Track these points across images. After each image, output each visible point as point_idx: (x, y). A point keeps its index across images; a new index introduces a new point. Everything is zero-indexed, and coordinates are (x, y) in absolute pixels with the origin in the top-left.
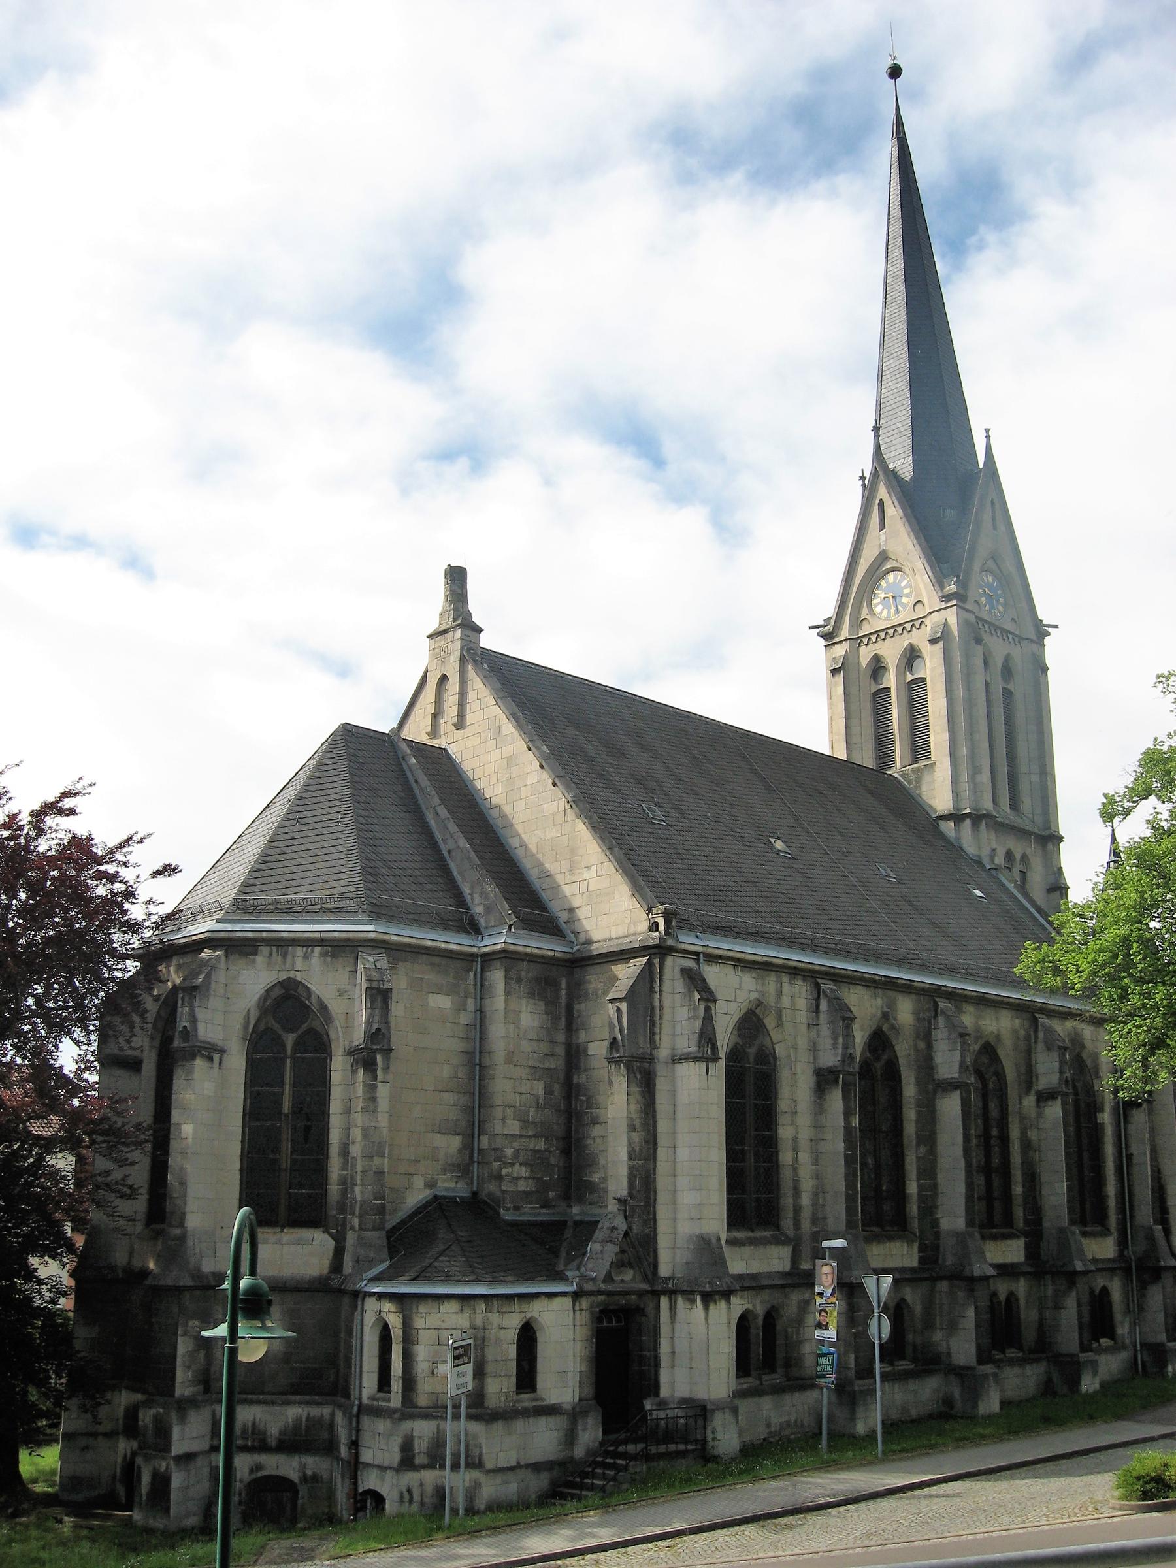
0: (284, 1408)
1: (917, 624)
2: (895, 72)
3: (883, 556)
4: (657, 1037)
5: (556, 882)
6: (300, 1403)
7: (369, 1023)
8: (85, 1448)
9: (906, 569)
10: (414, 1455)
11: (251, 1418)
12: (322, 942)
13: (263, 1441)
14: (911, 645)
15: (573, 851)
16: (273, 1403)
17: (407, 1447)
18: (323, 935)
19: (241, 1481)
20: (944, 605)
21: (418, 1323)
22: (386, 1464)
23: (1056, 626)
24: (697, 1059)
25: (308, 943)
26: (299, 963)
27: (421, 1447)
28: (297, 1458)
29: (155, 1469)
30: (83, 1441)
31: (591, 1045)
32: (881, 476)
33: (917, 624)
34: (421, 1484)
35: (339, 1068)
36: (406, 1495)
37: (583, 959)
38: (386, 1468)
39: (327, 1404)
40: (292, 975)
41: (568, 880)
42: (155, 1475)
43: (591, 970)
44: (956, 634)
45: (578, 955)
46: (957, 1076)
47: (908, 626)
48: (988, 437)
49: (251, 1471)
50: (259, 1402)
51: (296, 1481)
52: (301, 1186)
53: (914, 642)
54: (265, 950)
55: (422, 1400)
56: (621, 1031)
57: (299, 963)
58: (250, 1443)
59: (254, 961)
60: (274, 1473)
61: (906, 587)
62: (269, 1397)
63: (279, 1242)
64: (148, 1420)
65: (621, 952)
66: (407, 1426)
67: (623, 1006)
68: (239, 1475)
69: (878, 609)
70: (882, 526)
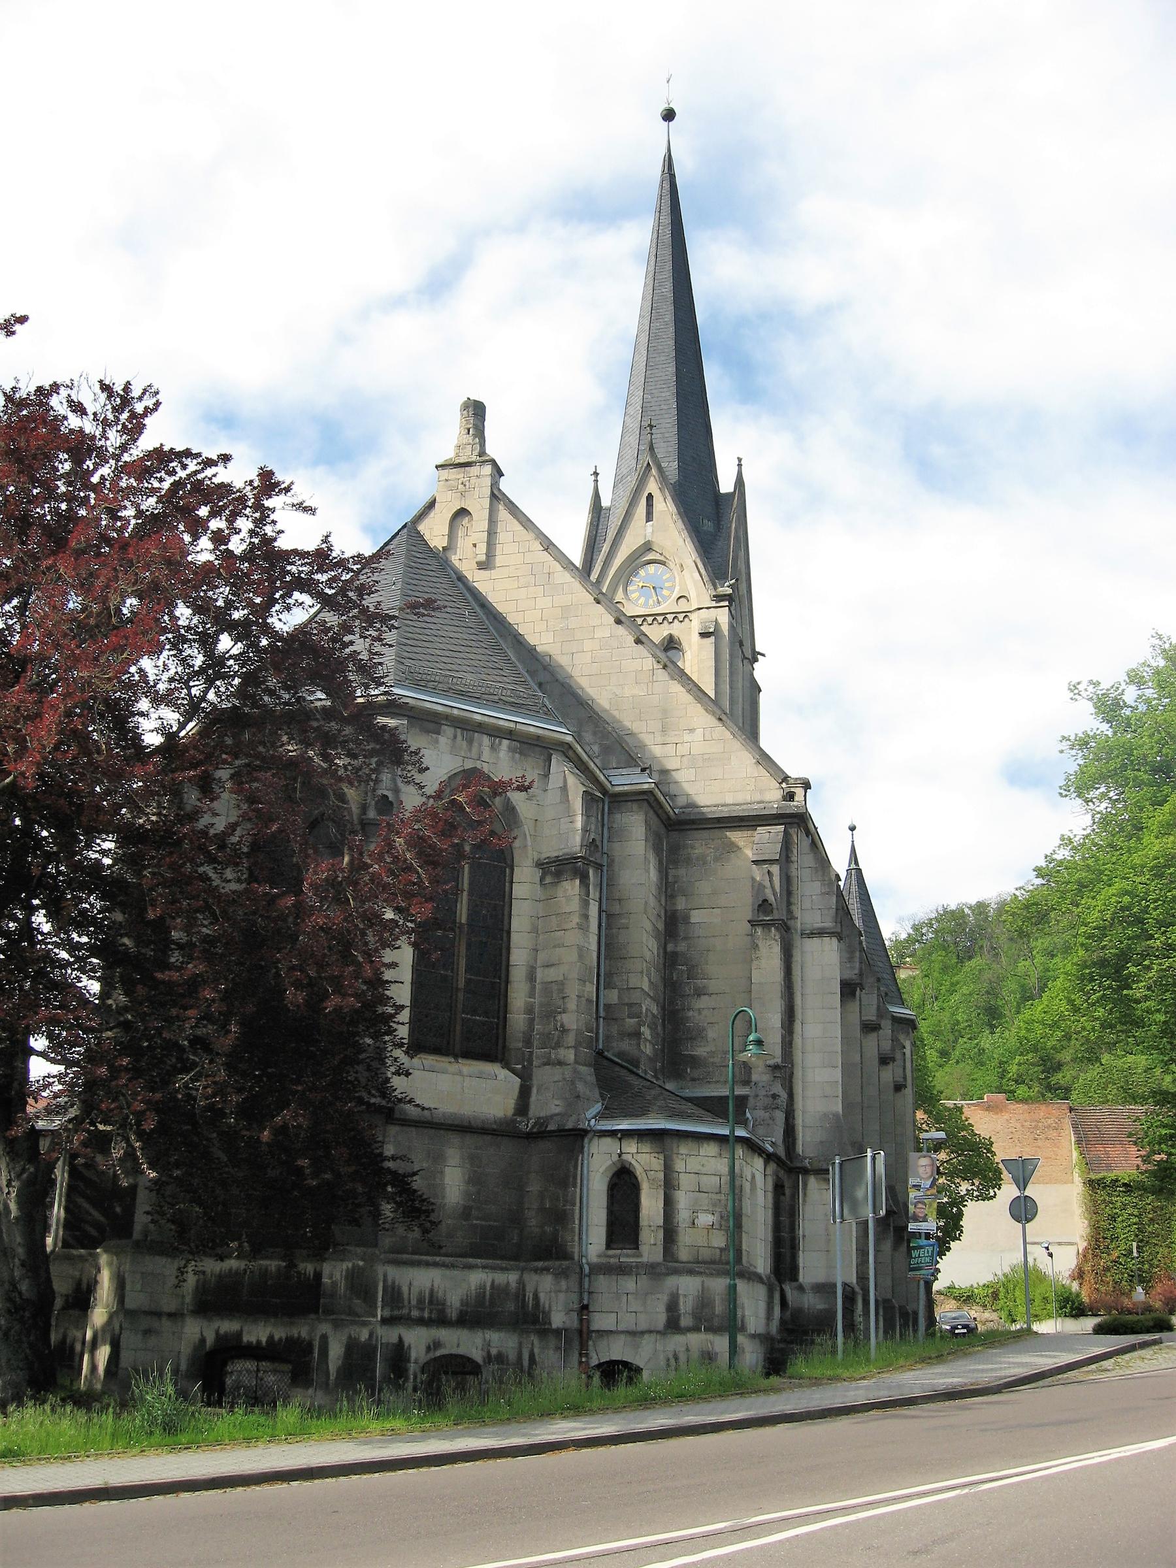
0: (466, 1272)
1: (681, 617)
2: (669, 115)
3: (647, 547)
4: (794, 908)
5: (640, 742)
6: (484, 1267)
7: (585, 830)
8: (147, 1332)
9: (672, 565)
10: (679, 1316)
11: (428, 1285)
12: (510, 734)
13: (442, 1312)
14: (671, 636)
15: (665, 713)
16: (453, 1266)
17: (672, 1307)
18: (519, 726)
19: (416, 1362)
20: (714, 604)
21: (679, 1166)
22: (643, 1326)
23: (763, 655)
24: (832, 934)
25: (497, 733)
26: (486, 754)
27: (686, 1306)
28: (480, 1334)
29: (350, 1337)
30: (145, 1322)
31: (693, 913)
32: (654, 471)
33: (681, 617)
34: (688, 1350)
35: (524, 883)
36: (672, 1361)
37: (693, 822)
38: (643, 1333)
39: (512, 1269)
40: (478, 765)
41: (659, 739)
42: (351, 1347)
43: (1082, 771)
44: (726, 633)
45: (683, 817)
46: (874, 1018)
47: (670, 617)
48: (740, 465)
49: (429, 1349)
50: (436, 1265)
51: (479, 1360)
52: (474, 1012)
53: (675, 633)
54: (448, 731)
55: (684, 1254)
56: (775, 894)
57: (486, 754)
58: (426, 1315)
59: (437, 742)
60: (454, 1351)
61: (667, 580)
62: (447, 1260)
63: (460, 1073)
64: (337, 1276)
65: (741, 819)
66: (672, 1282)
67: (775, 869)
68: (413, 1355)
69: (634, 596)
70: (649, 517)
